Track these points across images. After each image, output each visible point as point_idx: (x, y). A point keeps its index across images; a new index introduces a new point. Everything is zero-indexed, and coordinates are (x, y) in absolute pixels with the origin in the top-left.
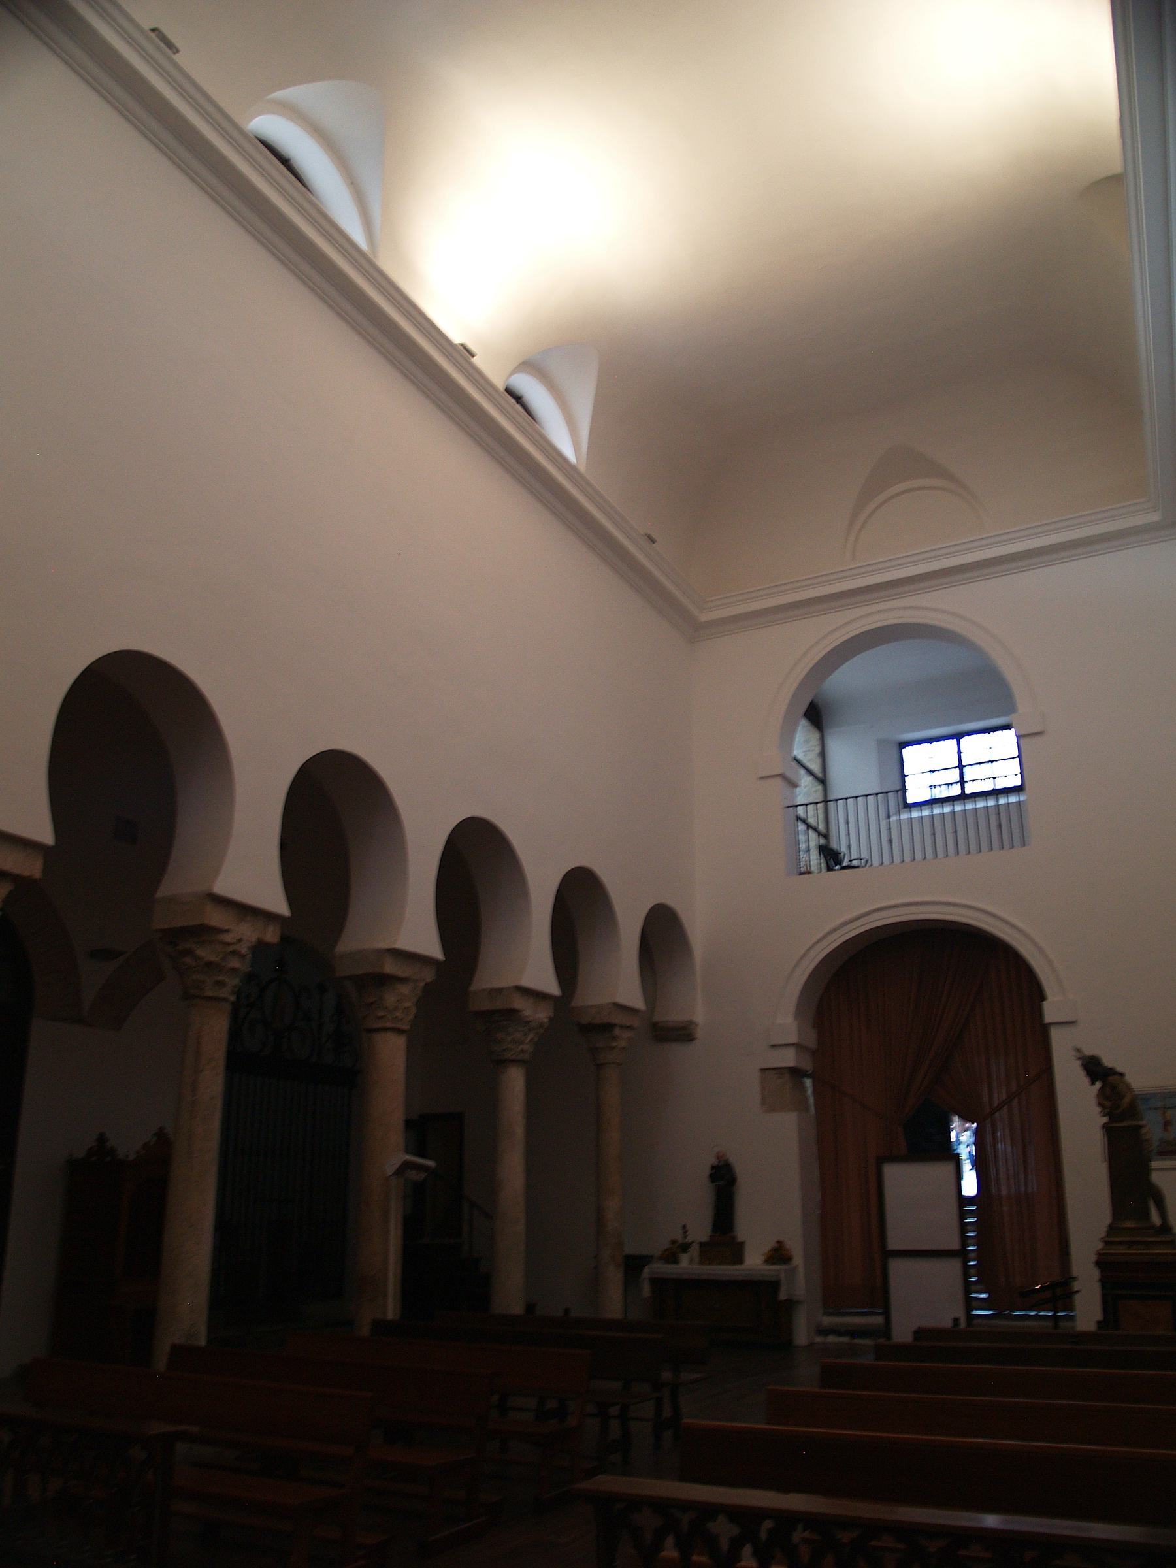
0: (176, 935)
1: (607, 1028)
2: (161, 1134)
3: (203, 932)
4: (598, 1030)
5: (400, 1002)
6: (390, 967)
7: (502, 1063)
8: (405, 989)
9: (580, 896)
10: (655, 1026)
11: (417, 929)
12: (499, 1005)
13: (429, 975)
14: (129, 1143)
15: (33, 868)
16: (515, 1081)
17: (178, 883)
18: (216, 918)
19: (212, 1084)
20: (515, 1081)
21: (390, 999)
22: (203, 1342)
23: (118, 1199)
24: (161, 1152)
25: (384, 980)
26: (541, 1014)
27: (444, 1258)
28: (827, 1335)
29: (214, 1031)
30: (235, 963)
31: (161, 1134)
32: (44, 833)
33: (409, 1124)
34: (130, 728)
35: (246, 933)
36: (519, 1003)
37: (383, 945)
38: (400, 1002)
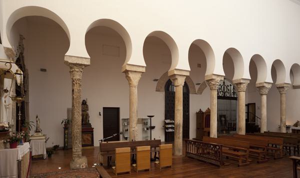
0: (208, 81)
1: (283, 87)
2: (208, 109)
3: (212, 80)
4: (281, 88)
5: (244, 87)
6: (242, 81)
7: (262, 95)
8: (244, 85)
9: (255, 63)
10: (293, 86)
11: (269, 79)
12: (261, 85)
13: (249, 82)
14: (204, 110)
15: (188, 74)
16: (264, 98)
17: (208, 73)
18: (214, 77)
19: (215, 101)
20: (264, 98)
21: (242, 86)
22: (216, 137)
23: (204, 118)
24: (209, 111)
25: (241, 83)
26: (269, 86)
27: (252, 127)
28: (19, 120)
29: (215, 94)
30: (217, 84)
31: (208, 109)
32: (250, 78)
33: (246, 105)
34: (38, 33)
35: (219, 79)
36: (265, 85)
37: (212, 73)
38: (244, 87)
